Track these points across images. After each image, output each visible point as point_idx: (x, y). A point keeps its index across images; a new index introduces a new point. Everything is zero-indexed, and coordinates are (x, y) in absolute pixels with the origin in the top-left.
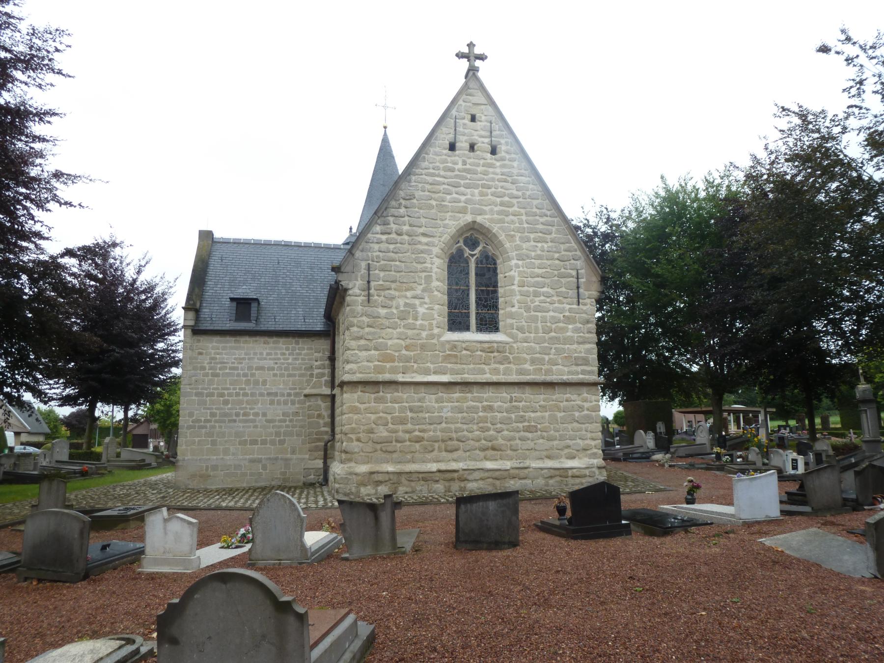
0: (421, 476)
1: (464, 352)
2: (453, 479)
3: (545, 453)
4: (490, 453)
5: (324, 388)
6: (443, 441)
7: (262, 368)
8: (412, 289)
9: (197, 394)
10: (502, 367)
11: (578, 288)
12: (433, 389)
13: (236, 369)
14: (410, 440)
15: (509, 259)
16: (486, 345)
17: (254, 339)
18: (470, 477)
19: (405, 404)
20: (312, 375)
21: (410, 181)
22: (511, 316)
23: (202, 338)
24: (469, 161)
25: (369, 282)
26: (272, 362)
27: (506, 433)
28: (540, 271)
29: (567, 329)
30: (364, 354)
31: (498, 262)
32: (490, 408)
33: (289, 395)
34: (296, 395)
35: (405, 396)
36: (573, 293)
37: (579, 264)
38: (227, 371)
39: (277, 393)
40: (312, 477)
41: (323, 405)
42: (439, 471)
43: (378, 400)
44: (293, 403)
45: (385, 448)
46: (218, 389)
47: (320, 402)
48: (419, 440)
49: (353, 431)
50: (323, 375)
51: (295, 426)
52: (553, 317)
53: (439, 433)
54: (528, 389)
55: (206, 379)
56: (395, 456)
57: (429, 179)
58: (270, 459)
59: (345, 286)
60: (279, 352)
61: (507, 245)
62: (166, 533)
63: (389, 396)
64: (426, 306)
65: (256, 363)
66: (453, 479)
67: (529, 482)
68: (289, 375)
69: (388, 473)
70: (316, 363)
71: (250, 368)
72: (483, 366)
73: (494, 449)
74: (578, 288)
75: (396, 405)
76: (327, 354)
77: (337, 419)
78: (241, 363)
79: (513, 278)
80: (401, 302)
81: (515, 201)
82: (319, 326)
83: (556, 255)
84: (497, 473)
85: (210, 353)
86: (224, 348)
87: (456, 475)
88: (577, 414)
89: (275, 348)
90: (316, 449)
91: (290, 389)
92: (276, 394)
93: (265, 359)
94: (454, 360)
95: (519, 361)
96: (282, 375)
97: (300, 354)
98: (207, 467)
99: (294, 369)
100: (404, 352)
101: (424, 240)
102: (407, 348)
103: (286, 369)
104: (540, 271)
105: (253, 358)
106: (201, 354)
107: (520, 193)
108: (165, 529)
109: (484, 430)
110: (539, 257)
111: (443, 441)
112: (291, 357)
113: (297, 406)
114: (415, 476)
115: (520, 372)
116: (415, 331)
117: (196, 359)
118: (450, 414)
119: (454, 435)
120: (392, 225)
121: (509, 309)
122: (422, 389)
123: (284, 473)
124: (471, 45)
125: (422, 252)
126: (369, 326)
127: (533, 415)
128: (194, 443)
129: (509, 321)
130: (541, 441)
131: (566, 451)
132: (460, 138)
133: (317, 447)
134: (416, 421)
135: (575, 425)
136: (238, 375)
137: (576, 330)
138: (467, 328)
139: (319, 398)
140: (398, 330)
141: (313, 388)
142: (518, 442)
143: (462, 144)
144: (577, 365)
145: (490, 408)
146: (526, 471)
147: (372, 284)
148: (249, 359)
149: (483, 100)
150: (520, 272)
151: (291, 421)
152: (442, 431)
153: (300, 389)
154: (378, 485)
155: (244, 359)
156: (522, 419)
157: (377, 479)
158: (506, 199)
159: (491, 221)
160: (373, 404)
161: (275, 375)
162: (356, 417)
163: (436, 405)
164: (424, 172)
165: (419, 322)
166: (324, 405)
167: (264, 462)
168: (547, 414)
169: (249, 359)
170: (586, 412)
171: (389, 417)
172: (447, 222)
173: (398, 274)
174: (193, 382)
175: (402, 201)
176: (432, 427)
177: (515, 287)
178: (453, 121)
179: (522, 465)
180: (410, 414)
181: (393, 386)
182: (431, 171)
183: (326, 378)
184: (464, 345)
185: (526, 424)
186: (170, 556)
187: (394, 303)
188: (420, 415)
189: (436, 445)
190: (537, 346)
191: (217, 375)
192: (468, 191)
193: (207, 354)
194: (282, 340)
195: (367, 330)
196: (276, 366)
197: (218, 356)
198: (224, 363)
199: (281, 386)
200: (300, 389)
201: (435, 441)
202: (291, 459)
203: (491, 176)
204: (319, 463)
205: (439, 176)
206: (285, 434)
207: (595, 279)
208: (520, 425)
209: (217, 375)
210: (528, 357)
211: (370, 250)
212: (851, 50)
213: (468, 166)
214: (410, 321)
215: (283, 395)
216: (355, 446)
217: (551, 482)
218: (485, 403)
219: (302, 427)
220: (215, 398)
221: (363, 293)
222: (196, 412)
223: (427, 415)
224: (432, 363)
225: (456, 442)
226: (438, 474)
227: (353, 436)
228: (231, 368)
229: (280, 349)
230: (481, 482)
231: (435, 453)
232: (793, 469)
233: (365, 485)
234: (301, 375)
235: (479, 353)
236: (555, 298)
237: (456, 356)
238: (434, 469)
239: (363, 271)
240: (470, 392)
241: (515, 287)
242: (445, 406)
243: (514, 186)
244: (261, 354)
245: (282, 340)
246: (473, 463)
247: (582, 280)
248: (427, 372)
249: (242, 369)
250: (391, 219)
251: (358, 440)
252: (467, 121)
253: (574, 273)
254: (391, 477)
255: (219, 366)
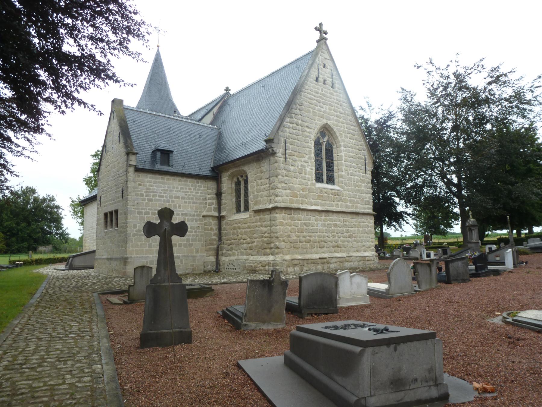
0: (312, 261)
1: (325, 194)
2: (324, 263)
3: (356, 249)
4: (336, 248)
5: (213, 212)
6: (319, 242)
7: (178, 197)
8: (304, 157)
9: (138, 213)
10: (339, 203)
11: (365, 165)
12: (314, 214)
13: (162, 197)
14: (305, 242)
15: (340, 146)
16: (333, 191)
17: (173, 178)
18: (332, 262)
19: (303, 221)
20: (206, 204)
21: (301, 95)
22: (342, 177)
23: (141, 174)
24: (324, 89)
25: (286, 150)
26: (183, 194)
27: (342, 238)
28: (352, 154)
29: (361, 186)
30: (284, 191)
31: (334, 147)
32: (335, 225)
33: (194, 215)
34: (198, 215)
35: (303, 217)
36: (363, 167)
37: (366, 153)
38: (157, 198)
39: (187, 214)
40: (210, 267)
41: (213, 222)
42: (320, 258)
43: (292, 219)
44: (196, 221)
45: (295, 246)
46: (152, 209)
47: (211, 221)
48: (309, 241)
49: (282, 236)
50: (212, 204)
51: (197, 235)
52: (357, 179)
53: (317, 238)
54: (349, 216)
55: (144, 202)
56: (299, 250)
57: (309, 96)
58: (184, 256)
59: (275, 151)
60: (187, 187)
61: (340, 139)
62: (351, 284)
63: (296, 216)
64: (310, 167)
65: (174, 193)
66: (324, 263)
67: (352, 263)
68: (194, 203)
69: (299, 259)
70: (210, 196)
71: (171, 197)
72: (332, 202)
73: (338, 247)
74: (365, 165)
75: (299, 222)
76: (215, 191)
77: (223, 232)
78: (166, 193)
79: (341, 156)
80: (299, 163)
81: (342, 115)
82: (207, 173)
83: (357, 147)
84: (341, 259)
85: (146, 185)
86: (155, 182)
87: (325, 260)
88: (366, 229)
89: (185, 185)
90: (210, 250)
91: (195, 212)
92: (186, 215)
93: (180, 191)
94: (321, 198)
95: (345, 201)
96: (190, 203)
97: (199, 190)
98: (147, 262)
99: (196, 199)
100: (301, 192)
101: (308, 130)
102: (303, 190)
103: (192, 199)
104: (352, 154)
105: (173, 190)
106: (140, 185)
107: (343, 112)
108: (351, 281)
109: (334, 236)
110: (351, 147)
111: (319, 242)
112: (194, 191)
113: (198, 222)
114: (310, 261)
115: (347, 207)
116: (305, 181)
117: (137, 188)
118: (321, 228)
119: (323, 239)
120: (294, 119)
121: (340, 173)
122: (310, 213)
123: (193, 265)
124: (321, 24)
125: (307, 137)
126: (286, 176)
127: (351, 229)
128: (137, 245)
129: (341, 179)
130: (354, 243)
131: (363, 248)
132: (320, 76)
133: (210, 248)
134: (308, 231)
135: (366, 234)
136: (164, 201)
137: (365, 187)
138: (322, 181)
139: (211, 218)
140: (299, 179)
141: (208, 211)
142: (346, 243)
143: (321, 80)
144: (366, 204)
145: (335, 225)
146: (351, 258)
147: (287, 151)
148: (170, 191)
149: (328, 57)
150: (345, 154)
151: (195, 232)
152: (318, 236)
153: (200, 212)
154: (294, 267)
155: (167, 190)
156: (348, 231)
157: (294, 263)
158: (338, 113)
159: (333, 124)
160: (289, 221)
161: (186, 202)
162: (282, 228)
163: (315, 222)
164: (307, 91)
165: (307, 176)
166: (214, 224)
167: (181, 258)
168: (356, 229)
169: (170, 191)
170: (369, 228)
171: (296, 228)
172: (316, 121)
173: (298, 148)
174: (136, 204)
175: (297, 105)
176: (314, 234)
177: (343, 161)
178: (317, 65)
179: (349, 255)
180: (305, 227)
181: (298, 211)
182: (309, 91)
183: (214, 206)
184: (325, 190)
185: (349, 234)
186: (355, 296)
187: (296, 164)
188: (309, 227)
189: (316, 244)
190: (352, 193)
191: (151, 200)
192: (324, 106)
193: (144, 185)
194: (189, 180)
195: (286, 178)
196: (186, 196)
197: (151, 187)
198: (155, 192)
199: (189, 210)
200: (200, 212)
201: (316, 242)
202: (196, 256)
203: (333, 100)
204: (213, 259)
205: (312, 95)
206: (193, 240)
207: (371, 162)
208: (347, 234)
209: (151, 200)
210: (349, 199)
211: (285, 131)
212: (430, 68)
213: (323, 92)
214: (303, 175)
215: (190, 215)
216: (282, 245)
217: (360, 263)
218: (334, 222)
219: (201, 236)
220: (150, 215)
221: (283, 156)
222: (138, 225)
223: (312, 228)
224: (313, 199)
225: (323, 243)
226: (319, 260)
227: (281, 239)
228: (160, 196)
229: (188, 186)
230: (335, 264)
231: (315, 249)
232: (427, 257)
233: (289, 267)
234: (200, 203)
235: (331, 195)
236: (358, 169)
237: (322, 196)
238: (318, 258)
239: (283, 144)
240: (328, 216)
241: (343, 161)
242: (318, 223)
243: (341, 107)
244: (177, 188)
245: (189, 180)
246: (331, 254)
247: (367, 161)
248: (311, 204)
249: (166, 198)
250: (293, 115)
251: (284, 241)
252: (322, 67)
253: (364, 157)
254: (300, 262)
255: (152, 194)
